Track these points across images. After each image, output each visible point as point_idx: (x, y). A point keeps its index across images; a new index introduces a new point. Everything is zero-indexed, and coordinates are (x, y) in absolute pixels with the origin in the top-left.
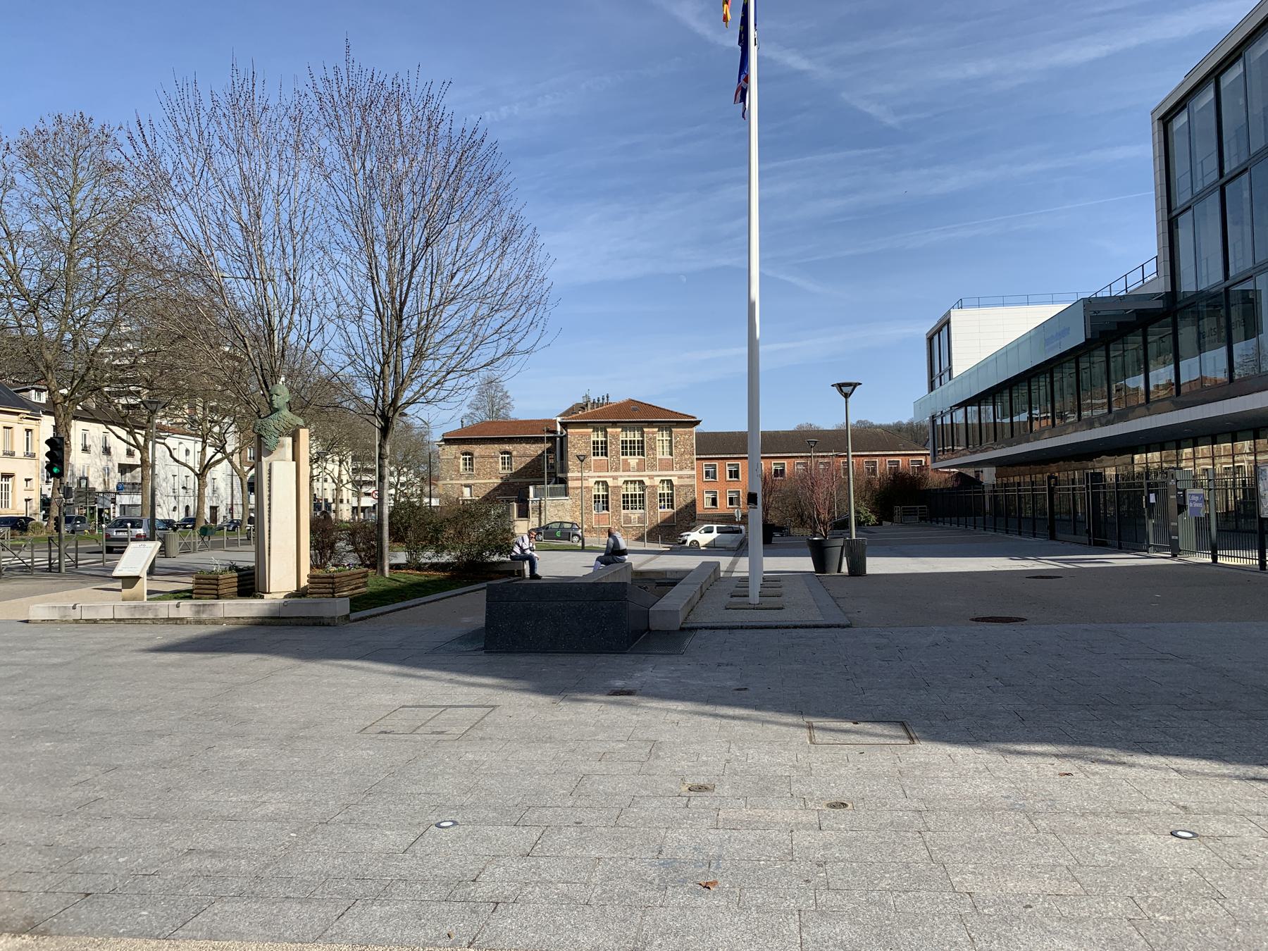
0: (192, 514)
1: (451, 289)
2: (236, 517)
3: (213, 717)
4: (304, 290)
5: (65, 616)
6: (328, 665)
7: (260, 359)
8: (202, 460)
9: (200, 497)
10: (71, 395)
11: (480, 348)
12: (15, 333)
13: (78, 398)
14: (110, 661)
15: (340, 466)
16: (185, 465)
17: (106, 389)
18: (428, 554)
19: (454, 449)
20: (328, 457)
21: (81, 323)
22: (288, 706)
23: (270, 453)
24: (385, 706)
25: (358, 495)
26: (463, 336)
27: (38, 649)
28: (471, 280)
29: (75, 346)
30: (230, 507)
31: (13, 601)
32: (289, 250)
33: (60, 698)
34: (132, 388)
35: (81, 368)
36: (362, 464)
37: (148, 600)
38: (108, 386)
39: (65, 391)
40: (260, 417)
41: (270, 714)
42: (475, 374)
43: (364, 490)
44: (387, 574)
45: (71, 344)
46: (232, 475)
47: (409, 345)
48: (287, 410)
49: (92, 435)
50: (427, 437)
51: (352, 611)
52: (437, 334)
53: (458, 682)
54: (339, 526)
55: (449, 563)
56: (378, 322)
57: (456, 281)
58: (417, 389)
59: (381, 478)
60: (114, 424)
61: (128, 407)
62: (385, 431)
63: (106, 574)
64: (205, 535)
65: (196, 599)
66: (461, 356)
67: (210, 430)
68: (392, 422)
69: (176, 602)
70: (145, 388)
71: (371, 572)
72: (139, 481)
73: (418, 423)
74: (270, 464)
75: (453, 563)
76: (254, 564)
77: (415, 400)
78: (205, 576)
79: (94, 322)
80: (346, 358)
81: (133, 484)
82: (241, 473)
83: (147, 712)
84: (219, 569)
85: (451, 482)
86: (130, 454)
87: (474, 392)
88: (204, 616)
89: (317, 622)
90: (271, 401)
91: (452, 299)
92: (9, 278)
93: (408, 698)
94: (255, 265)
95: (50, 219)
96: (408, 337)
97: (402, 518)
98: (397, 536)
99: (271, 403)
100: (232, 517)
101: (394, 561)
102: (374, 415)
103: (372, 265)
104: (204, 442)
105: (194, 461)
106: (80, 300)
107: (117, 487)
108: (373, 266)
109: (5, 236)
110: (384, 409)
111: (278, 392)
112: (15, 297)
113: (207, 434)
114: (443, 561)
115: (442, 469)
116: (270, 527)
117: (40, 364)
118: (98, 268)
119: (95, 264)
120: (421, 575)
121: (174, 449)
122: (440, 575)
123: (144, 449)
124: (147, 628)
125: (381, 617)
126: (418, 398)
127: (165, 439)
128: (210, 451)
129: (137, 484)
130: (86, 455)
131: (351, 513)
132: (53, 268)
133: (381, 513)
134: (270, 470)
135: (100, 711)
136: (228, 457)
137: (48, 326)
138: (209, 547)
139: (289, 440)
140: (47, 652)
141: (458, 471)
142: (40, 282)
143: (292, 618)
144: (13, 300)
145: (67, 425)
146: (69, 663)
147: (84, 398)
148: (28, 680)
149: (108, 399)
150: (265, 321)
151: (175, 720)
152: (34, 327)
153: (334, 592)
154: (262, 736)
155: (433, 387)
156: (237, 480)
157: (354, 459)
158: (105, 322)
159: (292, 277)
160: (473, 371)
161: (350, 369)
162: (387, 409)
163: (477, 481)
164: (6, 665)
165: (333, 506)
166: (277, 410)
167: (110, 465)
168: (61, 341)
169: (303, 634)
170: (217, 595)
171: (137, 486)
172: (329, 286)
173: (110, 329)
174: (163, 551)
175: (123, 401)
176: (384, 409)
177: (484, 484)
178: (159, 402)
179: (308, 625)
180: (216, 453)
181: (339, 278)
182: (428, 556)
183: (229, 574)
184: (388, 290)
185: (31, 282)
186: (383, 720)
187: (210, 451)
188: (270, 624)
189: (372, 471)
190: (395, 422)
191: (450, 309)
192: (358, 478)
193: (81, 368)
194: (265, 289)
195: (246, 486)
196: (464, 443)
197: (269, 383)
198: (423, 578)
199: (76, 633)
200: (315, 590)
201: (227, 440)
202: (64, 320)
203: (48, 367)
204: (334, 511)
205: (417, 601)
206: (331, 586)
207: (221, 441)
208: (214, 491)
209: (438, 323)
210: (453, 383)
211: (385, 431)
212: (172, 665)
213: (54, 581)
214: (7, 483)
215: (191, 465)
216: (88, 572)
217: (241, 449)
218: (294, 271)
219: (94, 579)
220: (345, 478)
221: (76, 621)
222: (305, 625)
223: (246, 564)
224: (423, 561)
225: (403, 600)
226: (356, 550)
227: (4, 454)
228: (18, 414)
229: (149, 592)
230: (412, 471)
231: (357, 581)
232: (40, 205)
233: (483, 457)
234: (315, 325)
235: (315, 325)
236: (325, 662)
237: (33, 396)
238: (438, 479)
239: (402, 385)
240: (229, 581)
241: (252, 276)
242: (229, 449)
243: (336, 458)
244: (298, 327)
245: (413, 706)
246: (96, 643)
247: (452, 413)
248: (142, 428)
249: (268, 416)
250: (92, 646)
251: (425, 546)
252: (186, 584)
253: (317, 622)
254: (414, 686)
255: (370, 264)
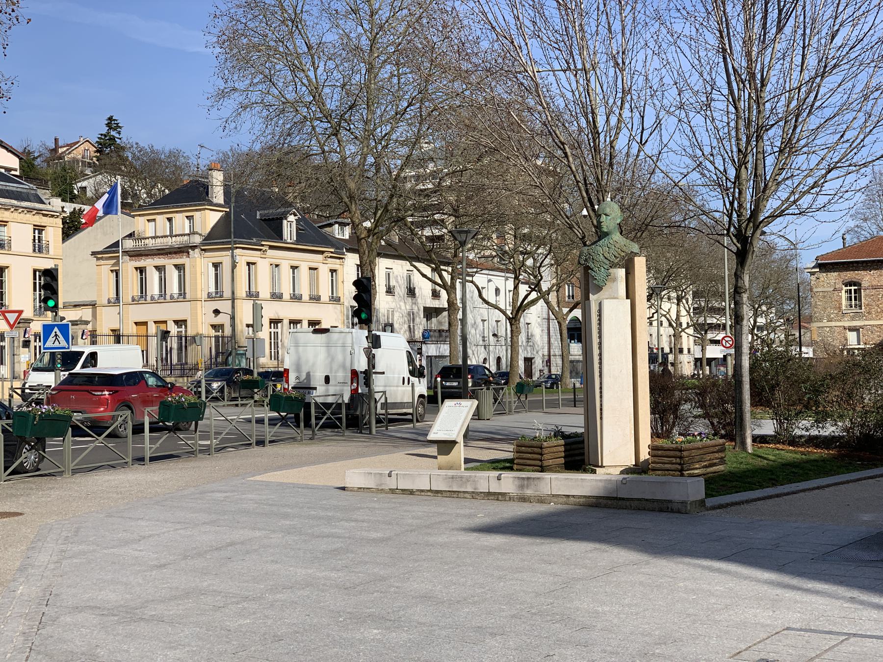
0: (504, 368)
1: (832, 53)
2: (554, 371)
3: (549, 618)
4: (636, 77)
5: (381, 485)
6: (684, 563)
7: (583, 170)
8: (515, 300)
9: (513, 346)
10: (375, 228)
11: (874, 131)
12: (318, 160)
13: (382, 231)
14: (431, 539)
15: (678, 304)
16: (496, 307)
17: (410, 219)
18: (805, 423)
19: (833, 278)
20: (663, 293)
21: (383, 143)
22: (637, 614)
23: (599, 289)
24: (763, 626)
25: (702, 343)
26: (850, 116)
27: (356, 521)
28: (860, 37)
29: (378, 170)
30: (546, 358)
31: (328, 465)
32: (617, 26)
33: (383, 579)
34: (437, 217)
35: (383, 196)
36: (707, 302)
37: (465, 469)
38: (412, 215)
39: (368, 224)
40: (585, 245)
41: (615, 621)
42: (868, 170)
43: (710, 336)
44: (750, 449)
45: (373, 169)
46: (549, 319)
47: (774, 136)
48: (618, 234)
49: (396, 273)
50: (794, 263)
51: (708, 495)
52: (812, 117)
53: (862, 603)
54: (682, 383)
55: (834, 437)
56: (732, 109)
57: (838, 41)
58: (786, 195)
59: (738, 318)
60: (419, 260)
61: (433, 239)
62: (742, 256)
63: (421, 439)
64: (522, 393)
65: (517, 470)
66: (847, 145)
67: (523, 264)
68: (751, 243)
69: (496, 473)
70: (450, 215)
71: (728, 445)
72: (445, 327)
73: (782, 244)
74: (600, 304)
75: (841, 437)
76: (582, 430)
77: (783, 211)
78: (527, 442)
79: (396, 141)
80: (689, 161)
81: (439, 331)
82: (560, 316)
83: (474, 603)
84: (543, 434)
85: (830, 324)
86: (435, 295)
87: (860, 197)
88: (529, 492)
89: (664, 507)
90: (599, 223)
91: (835, 66)
92: (312, 98)
93: (794, 618)
94: (576, 52)
95: (349, 25)
96: (773, 125)
97: (767, 373)
98: (759, 399)
99: (598, 226)
100: (550, 371)
101: (758, 432)
102: (728, 235)
103: (724, 33)
104: (516, 278)
105: (505, 302)
106: (381, 116)
107: (423, 335)
108: (725, 34)
109: (306, 50)
110: (740, 226)
111: (608, 211)
112: (318, 119)
113: (520, 268)
114: (827, 434)
115: (817, 305)
116: (601, 383)
117: (343, 194)
118: (399, 76)
119: (396, 73)
120: (796, 453)
121: (483, 288)
122: (817, 453)
123: (450, 289)
124: (464, 502)
125: (746, 506)
126: (787, 209)
127: (473, 276)
128: (523, 289)
129: (443, 331)
130: (390, 298)
131: (693, 367)
132: (354, 82)
133: (738, 367)
134: (600, 312)
135: (425, 598)
136: (544, 296)
137: (351, 149)
138: (527, 409)
139: (621, 273)
140: (365, 524)
141: (840, 308)
142: (341, 99)
143: (632, 499)
144: (316, 123)
145: (372, 264)
146: (389, 539)
147: (388, 231)
148: (351, 556)
149: (412, 231)
150: (588, 122)
151: (506, 617)
152: (336, 152)
153: (681, 470)
154: (609, 648)
155: (808, 192)
156: (554, 324)
157: (696, 295)
158: (407, 139)
159: (620, 61)
160: (865, 165)
161: (695, 176)
162: (744, 225)
163: (867, 323)
164: (328, 536)
165: (671, 358)
166: (606, 234)
167: (415, 309)
168: (364, 166)
169: (645, 521)
170: (541, 466)
171: (444, 334)
172: (668, 66)
173: (413, 148)
174: (478, 415)
175: (427, 232)
176: (740, 226)
177: (877, 326)
178: (467, 232)
179: (653, 510)
180: (531, 292)
181: (681, 55)
182: (804, 427)
183: (554, 442)
184: (744, 64)
185: (333, 101)
186: (762, 644)
187: (523, 289)
188: (606, 506)
189: (720, 311)
190: (755, 243)
191: (831, 81)
192: (701, 320)
193: (383, 196)
194: (588, 81)
195: (565, 332)
196: (847, 270)
197: (595, 201)
198: (798, 456)
199: (393, 505)
200: (658, 466)
201: (543, 274)
202: (366, 142)
203: (351, 197)
204: (673, 364)
205: (787, 488)
206: (678, 460)
207: (535, 277)
208: (528, 339)
209: (814, 102)
210: (837, 183)
211: (742, 256)
212: (498, 549)
213: (365, 444)
214: (276, 330)
215: (502, 307)
216: (399, 435)
217: (559, 287)
218: (623, 53)
219: (405, 442)
220: (685, 320)
221: (392, 491)
222: (649, 510)
223: (573, 430)
224: (798, 432)
225: (774, 485)
226: (706, 416)
227: (311, 299)
228: (322, 252)
229: (467, 461)
230: (773, 310)
231: (712, 456)
232: (339, 10)
233: (875, 288)
234: (649, 121)
235: (649, 121)
236: (679, 560)
237: (337, 232)
238: (810, 319)
239: (764, 191)
240: (555, 449)
241: (572, 67)
242: (545, 286)
243: (673, 295)
244: (630, 126)
245: (801, 630)
246: (413, 518)
247: (835, 226)
248: (448, 264)
249: (596, 242)
250: (410, 521)
251: (800, 412)
252: (505, 452)
253: (664, 507)
254: (801, 602)
255: (721, 32)
